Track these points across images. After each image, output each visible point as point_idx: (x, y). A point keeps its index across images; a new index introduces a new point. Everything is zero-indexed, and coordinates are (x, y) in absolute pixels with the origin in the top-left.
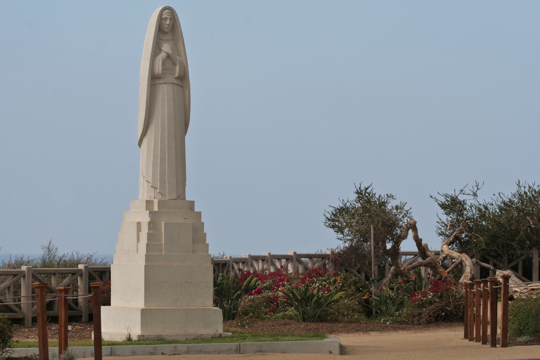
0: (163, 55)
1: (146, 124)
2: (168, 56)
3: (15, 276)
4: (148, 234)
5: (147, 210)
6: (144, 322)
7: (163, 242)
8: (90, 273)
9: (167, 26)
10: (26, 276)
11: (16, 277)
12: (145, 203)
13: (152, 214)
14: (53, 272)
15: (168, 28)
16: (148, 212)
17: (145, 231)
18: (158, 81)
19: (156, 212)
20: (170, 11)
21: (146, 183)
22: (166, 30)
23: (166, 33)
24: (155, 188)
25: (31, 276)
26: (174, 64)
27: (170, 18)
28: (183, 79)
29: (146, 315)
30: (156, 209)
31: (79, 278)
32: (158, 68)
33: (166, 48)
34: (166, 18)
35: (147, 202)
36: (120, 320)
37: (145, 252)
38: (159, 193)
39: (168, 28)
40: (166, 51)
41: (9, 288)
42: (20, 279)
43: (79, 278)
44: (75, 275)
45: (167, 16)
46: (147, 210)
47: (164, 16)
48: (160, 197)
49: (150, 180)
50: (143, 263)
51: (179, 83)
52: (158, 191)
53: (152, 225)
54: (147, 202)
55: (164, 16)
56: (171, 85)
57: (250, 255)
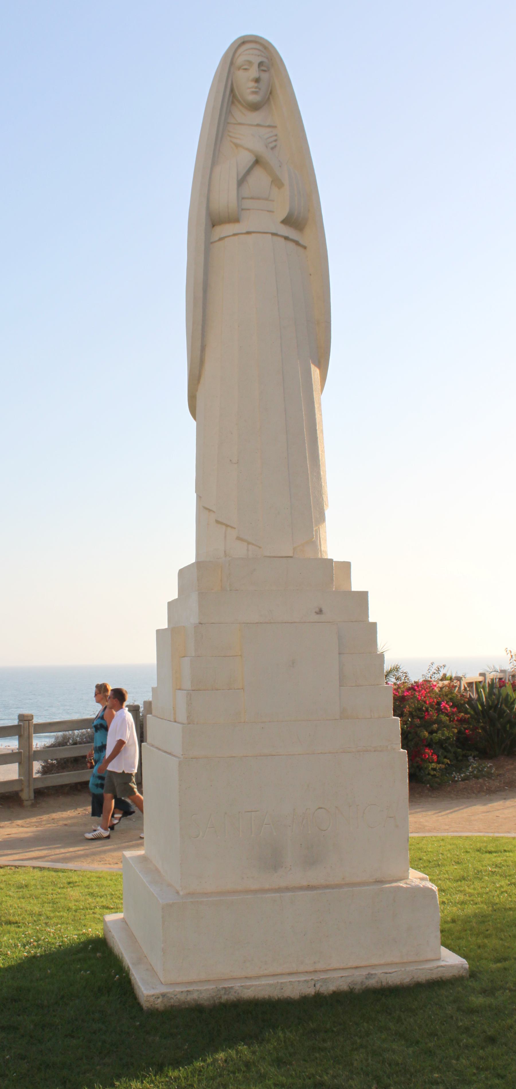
15: (252, 89)
24: (227, 526)
34: (250, 63)
39: (252, 89)
47: (240, 60)
55: (240, 60)
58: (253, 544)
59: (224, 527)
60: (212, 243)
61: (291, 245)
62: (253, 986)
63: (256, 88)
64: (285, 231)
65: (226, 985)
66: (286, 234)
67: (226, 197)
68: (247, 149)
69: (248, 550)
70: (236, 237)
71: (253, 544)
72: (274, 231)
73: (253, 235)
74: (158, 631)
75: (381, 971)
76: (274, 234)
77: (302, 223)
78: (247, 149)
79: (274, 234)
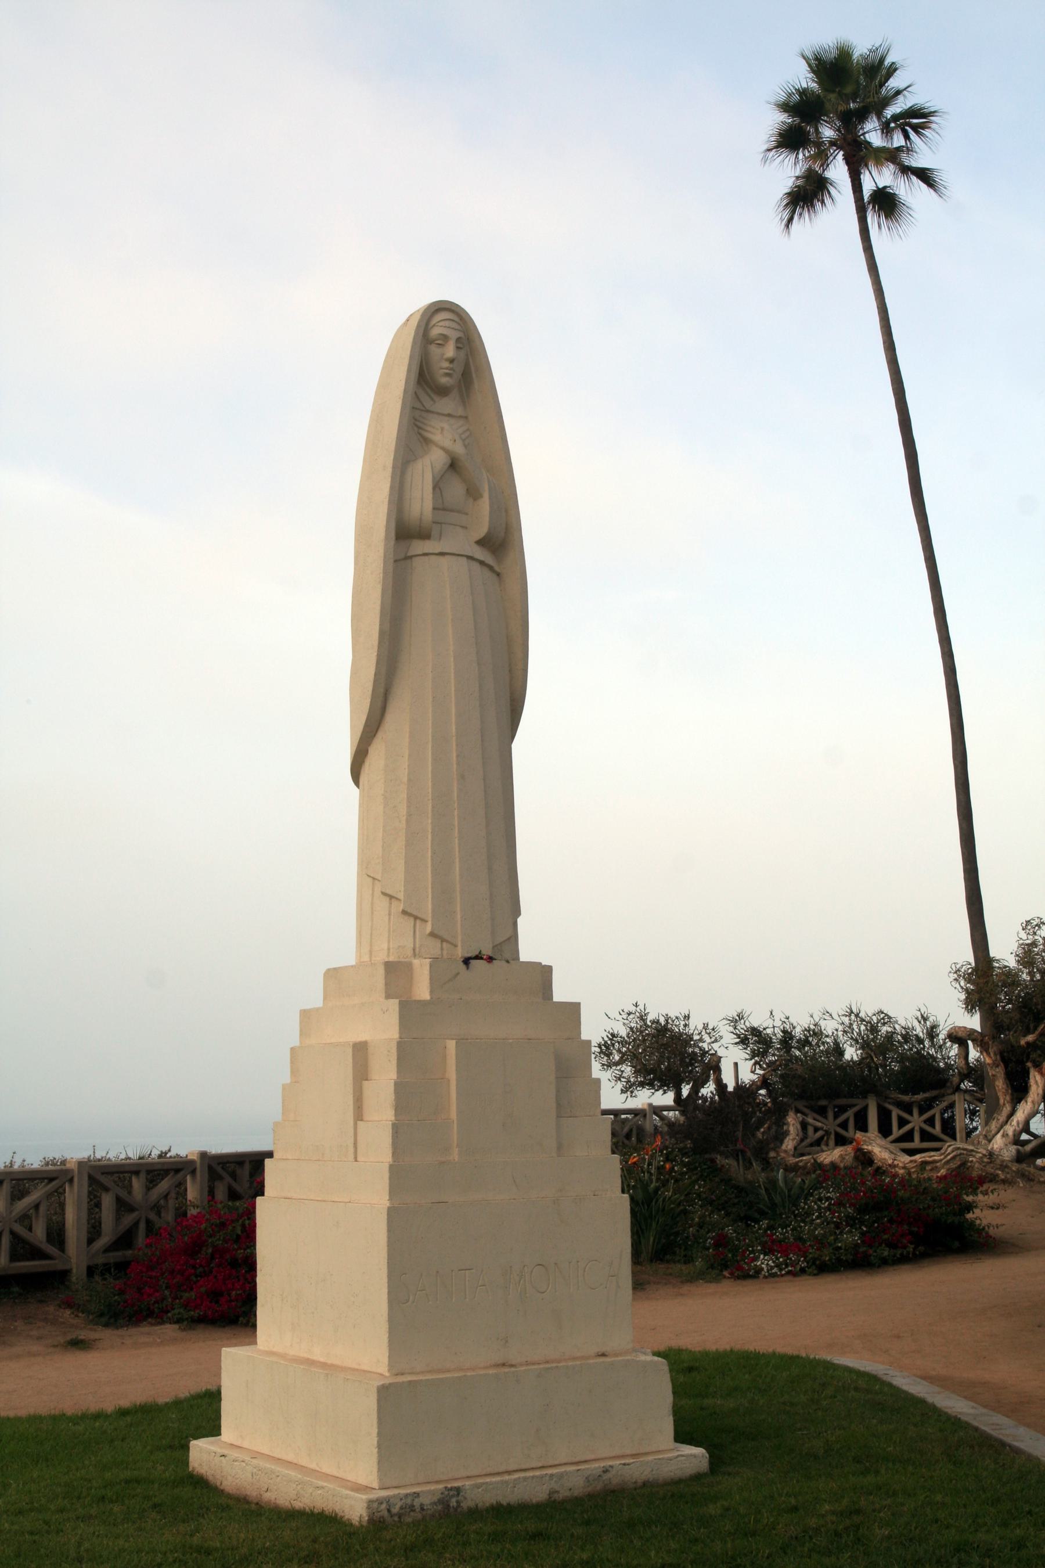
0: (433, 460)
1: (382, 690)
2: (454, 465)
3: (51, 1180)
4: (400, 1088)
5: (388, 996)
6: (390, 1444)
7: (454, 1114)
8: (210, 1168)
9: (446, 364)
10: (76, 1180)
11: (54, 1183)
12: (381, 971)
13: (410, 1012)
14: (134, 1169)
15: (445, 374)
16: (394, 1004)
17: (385, 1075)
18: (419, 547)
19: (423, 1004)
20: (423, 432)
21: (383, 903)
22: (444, 381)
23: (443, 392)
24: (416, 918)
25: (86, 1178)
26: (473, 493)
27: (458, 340)
28: (501, 545)
29: (399, 1407)
30: (422, 991)
31: (189, 1178)
32: (421, 503)
33: (445, 435)
34: (445, 338)
35: (390, 968)
36: (299, 1405)
37: (386, 1157)
38: (432, 934)
39: (445, 374)
40: (447, 443)
41: (37, 1207)
42: (62, 1186)
43: (189, 1178)
44: (181, 1173)
45: (445, 331)
46: (388, 996)
47: (435, 332)
48: (434, 947)
49: (398, 888)
50: (383, 1201)
51: (489, 559)
52: (429, 928)
53: (409, 1052)
54: (390, 968)
55: (435, 332)
56: (465, 559)
57: (650, 1105)
58: (447, 941)
59: (412, 920)
60: (411, 557)
61: (487, 573)
62: (483, 1484)
63: (451, 369)
64: (480, 553)
65: (456, 1484)
66: (482, 558)
67: (421, 503)
68: (443, 449)
69: (442, 949)
70: (426, 558)
71: (447, 941)
72: (470, 554)
73: (447, 557)
74: (547, 971)
75: (618, 1462)
76: (470, 558)
77: (500, 545)
78: (443, 449)
79: (470, 558)
